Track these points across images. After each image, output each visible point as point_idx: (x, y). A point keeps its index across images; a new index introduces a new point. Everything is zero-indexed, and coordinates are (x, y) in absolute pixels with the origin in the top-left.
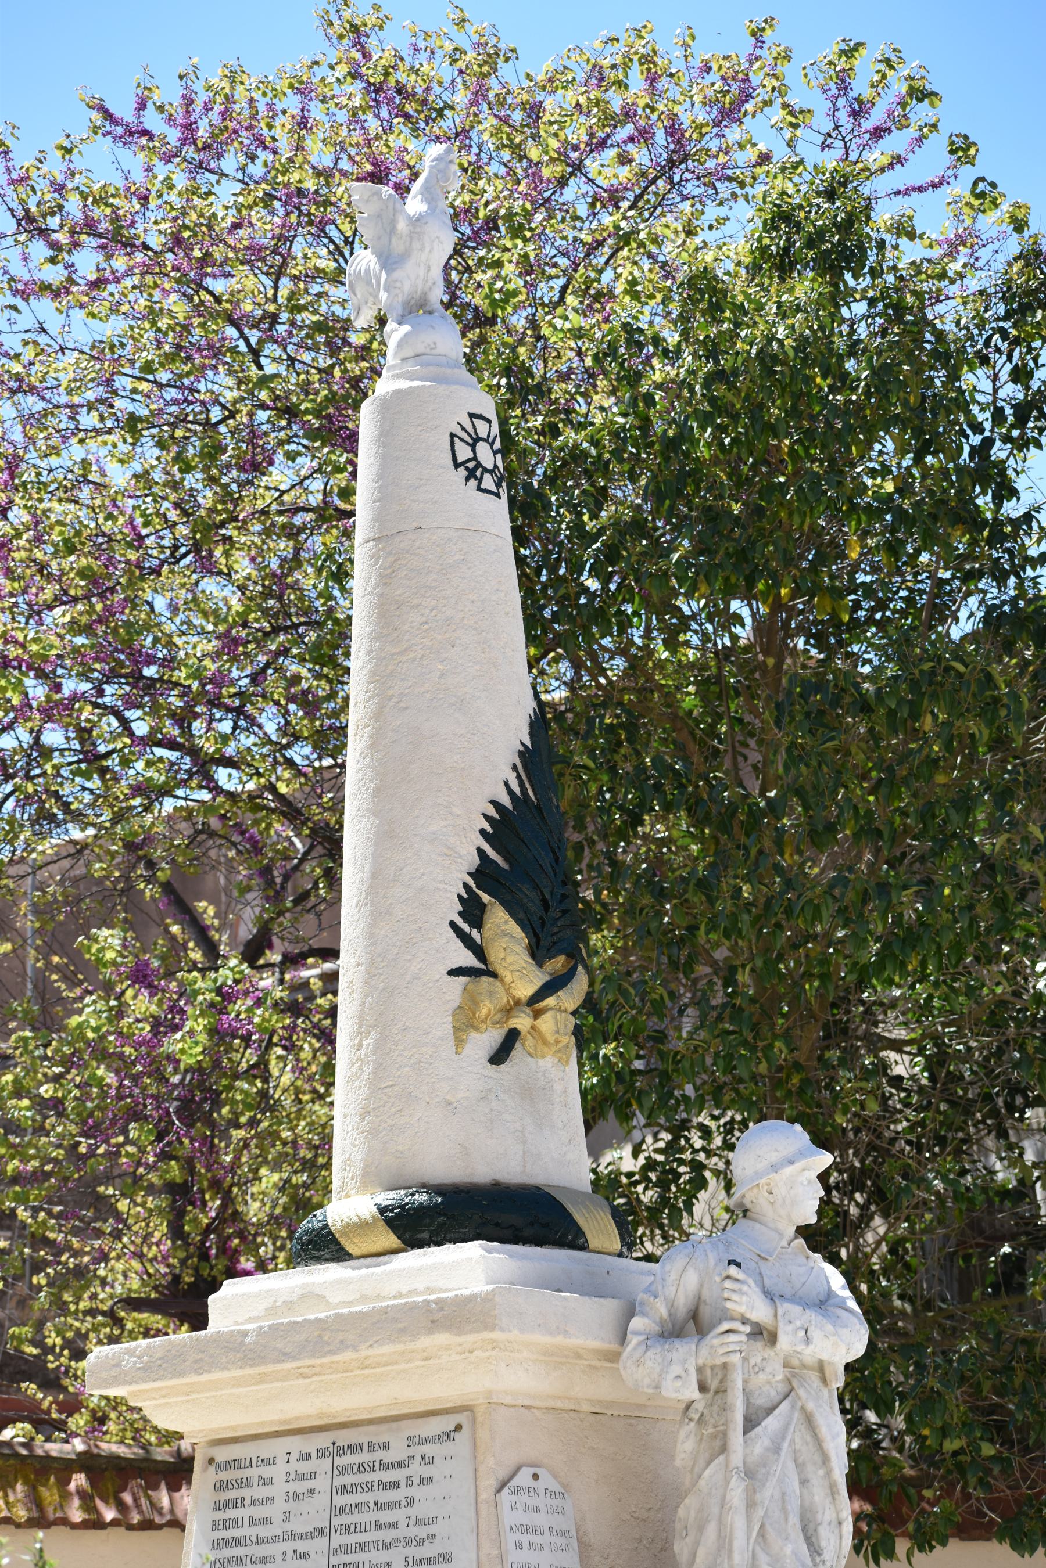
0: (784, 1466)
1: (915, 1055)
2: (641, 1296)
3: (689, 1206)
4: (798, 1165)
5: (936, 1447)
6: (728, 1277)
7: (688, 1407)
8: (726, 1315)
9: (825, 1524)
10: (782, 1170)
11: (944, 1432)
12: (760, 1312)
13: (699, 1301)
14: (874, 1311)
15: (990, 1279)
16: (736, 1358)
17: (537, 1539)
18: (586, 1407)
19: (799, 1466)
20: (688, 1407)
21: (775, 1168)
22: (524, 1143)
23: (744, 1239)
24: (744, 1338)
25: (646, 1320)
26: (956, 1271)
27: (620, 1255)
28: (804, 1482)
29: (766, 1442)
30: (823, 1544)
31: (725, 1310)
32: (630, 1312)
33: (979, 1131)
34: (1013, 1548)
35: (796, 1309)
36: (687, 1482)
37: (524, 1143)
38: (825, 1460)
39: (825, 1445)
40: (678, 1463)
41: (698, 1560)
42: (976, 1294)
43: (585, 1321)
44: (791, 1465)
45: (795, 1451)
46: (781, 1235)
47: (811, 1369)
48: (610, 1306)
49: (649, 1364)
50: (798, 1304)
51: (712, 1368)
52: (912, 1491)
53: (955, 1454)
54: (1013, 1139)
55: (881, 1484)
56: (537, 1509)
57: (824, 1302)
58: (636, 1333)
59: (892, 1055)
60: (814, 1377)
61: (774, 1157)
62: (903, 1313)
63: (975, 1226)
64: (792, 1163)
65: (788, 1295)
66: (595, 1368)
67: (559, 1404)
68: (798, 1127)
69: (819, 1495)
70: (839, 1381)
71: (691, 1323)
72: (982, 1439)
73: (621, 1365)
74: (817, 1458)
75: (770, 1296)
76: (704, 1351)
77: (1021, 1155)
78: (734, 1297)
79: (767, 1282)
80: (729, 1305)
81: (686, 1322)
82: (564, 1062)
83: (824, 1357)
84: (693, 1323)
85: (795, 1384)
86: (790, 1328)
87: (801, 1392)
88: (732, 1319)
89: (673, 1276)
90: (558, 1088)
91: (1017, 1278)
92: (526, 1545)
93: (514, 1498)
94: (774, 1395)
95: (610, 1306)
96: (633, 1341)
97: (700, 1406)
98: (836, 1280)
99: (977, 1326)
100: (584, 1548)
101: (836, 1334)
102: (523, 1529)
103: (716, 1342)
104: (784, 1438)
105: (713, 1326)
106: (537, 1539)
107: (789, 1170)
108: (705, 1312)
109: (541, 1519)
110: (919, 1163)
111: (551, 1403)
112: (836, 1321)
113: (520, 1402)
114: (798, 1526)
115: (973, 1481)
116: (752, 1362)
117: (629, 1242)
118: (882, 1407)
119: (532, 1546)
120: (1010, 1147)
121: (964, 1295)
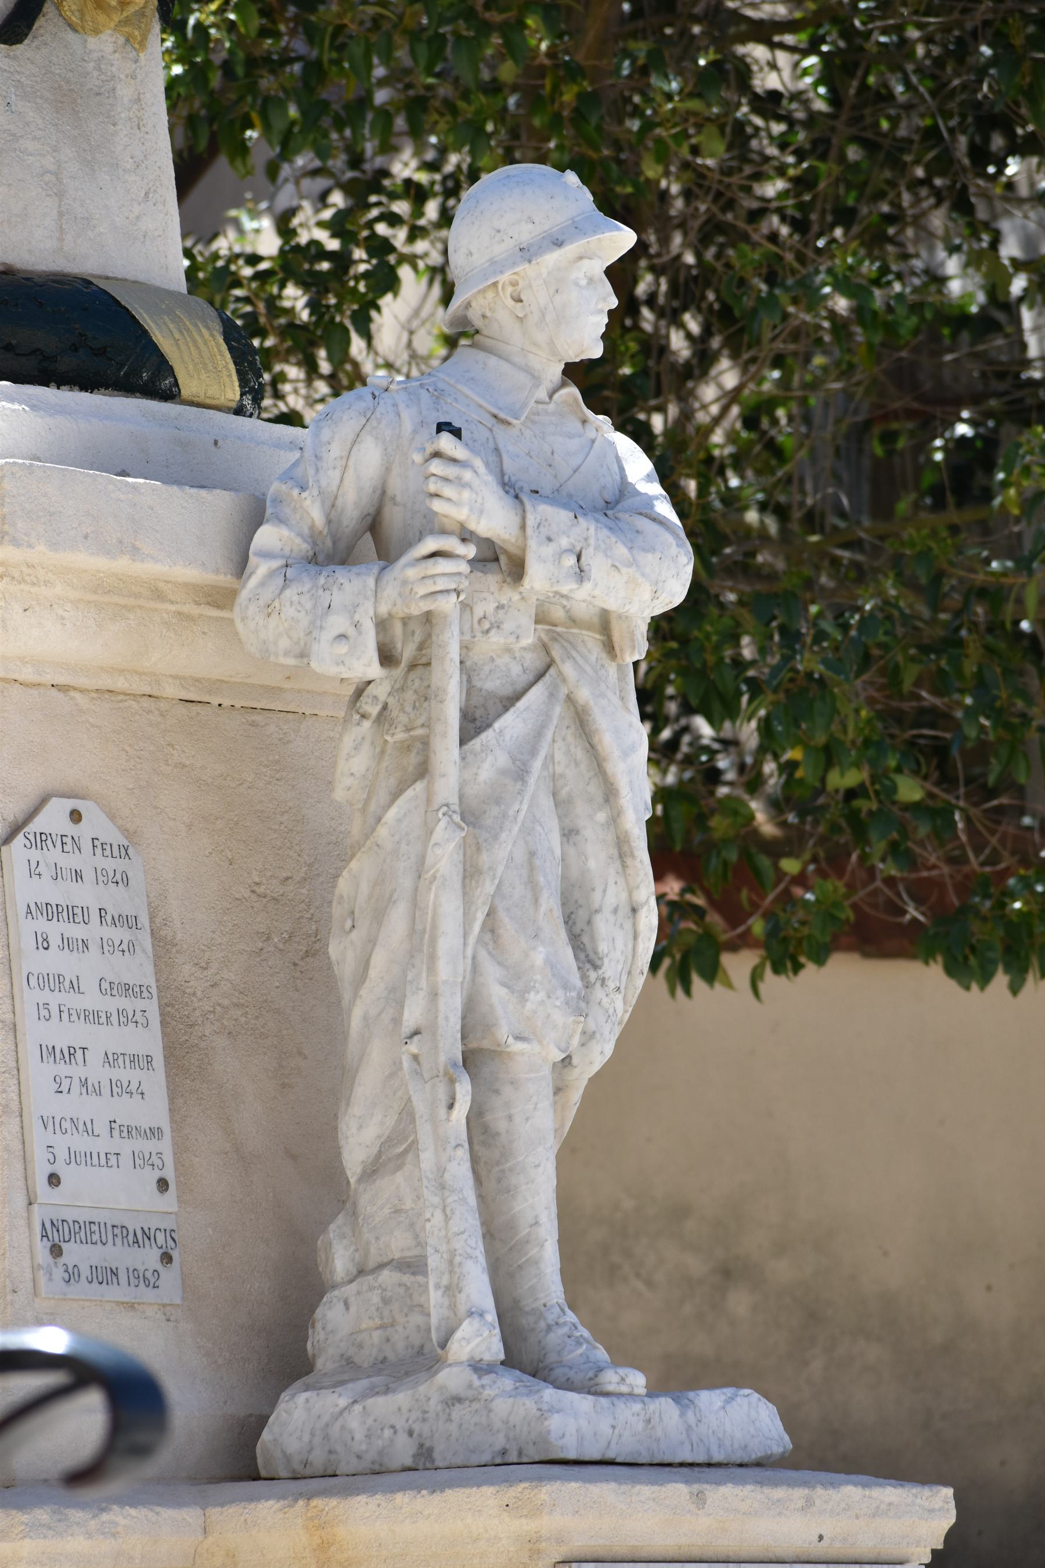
0: (534, 801)
1: (805, 53)
2: (275, 487)
3: (364, 325)
4: (570, 250)
5: (813, 781)
6: (437, 455)
7: (359, 693)
8: (433, 526)
9: (607, 912)
10: (539, 258)
11: (829, 755)
12: (495, 520)
13: (382, 498)
14: (707, 531)
15: (928, 479)
16: (448, 605)
17: (76, 931)
18: (172, 690)
19: (562, 804)
20: (359, 693)
21: (527, 253)
22: (60, 195)
23: (472, 373)
24: (464, 567)
25: (285, 532)
26: (866, 463)
27: (239, 411)
28: (569, 834)
29: (502, 759)
30: (603, 947)
31: (430, 516)
32: (256, 515)
33: (917, 200)
34: (951, 971)
35: (564, 516)
36: (356, 829)
37: (60, 195)
38: (610, 794)
39: (609, 767)
40: (339, 794)
41: (372, 973)
42: (903, 506)
43: (171, 531)
44: (546, 803)
45: (554, 777)
46: (536, 379)
47: (589, 627)
48: (217, 506)
49: (289, 612)
50: (565, 506)
51: (405, 621)
52: (764, 862)
53: (851, 794)
54: (982, 213)
55: (711, 846)
56: (78, 875)
57: (613, 505)
58: (267, 555)
59: (758, 52)
60: (592, 641)
61: (526, 234)
62: (763, 535)
63: (903, 376)
64: (559, 244)
65: (546, 489)
66: (189, 618)
67: (120, 684)
68: (571, 178)
69: (596, 857)
70: (637, 648)
71: (368, 535)
72: (899, 770)
73: (236, 614)
74: (595, 789)
75: (513, 490)
76: (390, 591)
77: (995, 244)
78: (448, 491)
79: (508, 464)
80: (437, 506)
81: (357, 536)
82: (136, 43)
83: (612, 604)
84: (370, 538)
85: (556, 653)
86: (549, 550)
87: (568, 669)
88: (443, 532)
89: (336, 450)
90: (125, 92)
91: (980, 478)
92: (55, 941)
93: (35, 855)
94: (518, 673)
95: (217, 506)
96: (260, 569)
97: (381, 691)
98: (637, 466)
99: (897, 562)
100: (163, 947)
101: (633, 563)
102: (50, 911)
103: (412, 573)
104: (533, 752)
105: (408, 545)
106: (76, 931)
107: (552, 258)
108: (394, 518)
109: (86, 895)
110: (801, 258)
111: (106, 682)
112: (633, 539)
113: (49, 678)
114: (558, 913)
115: (878, 847)
116: (479, 612)
117: (255, 383)
118: (717, 707)
119: (67, 943)
120: (975, 229)
121: (882, 508)
